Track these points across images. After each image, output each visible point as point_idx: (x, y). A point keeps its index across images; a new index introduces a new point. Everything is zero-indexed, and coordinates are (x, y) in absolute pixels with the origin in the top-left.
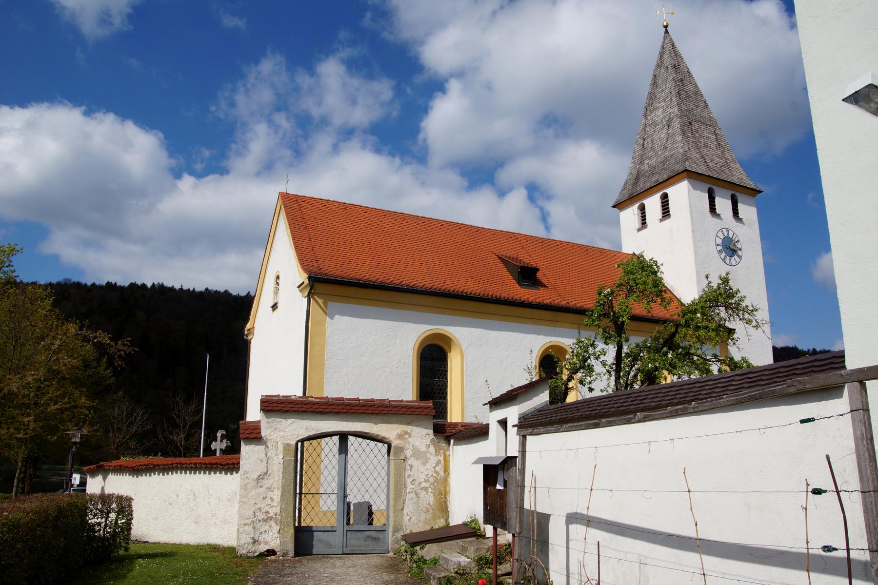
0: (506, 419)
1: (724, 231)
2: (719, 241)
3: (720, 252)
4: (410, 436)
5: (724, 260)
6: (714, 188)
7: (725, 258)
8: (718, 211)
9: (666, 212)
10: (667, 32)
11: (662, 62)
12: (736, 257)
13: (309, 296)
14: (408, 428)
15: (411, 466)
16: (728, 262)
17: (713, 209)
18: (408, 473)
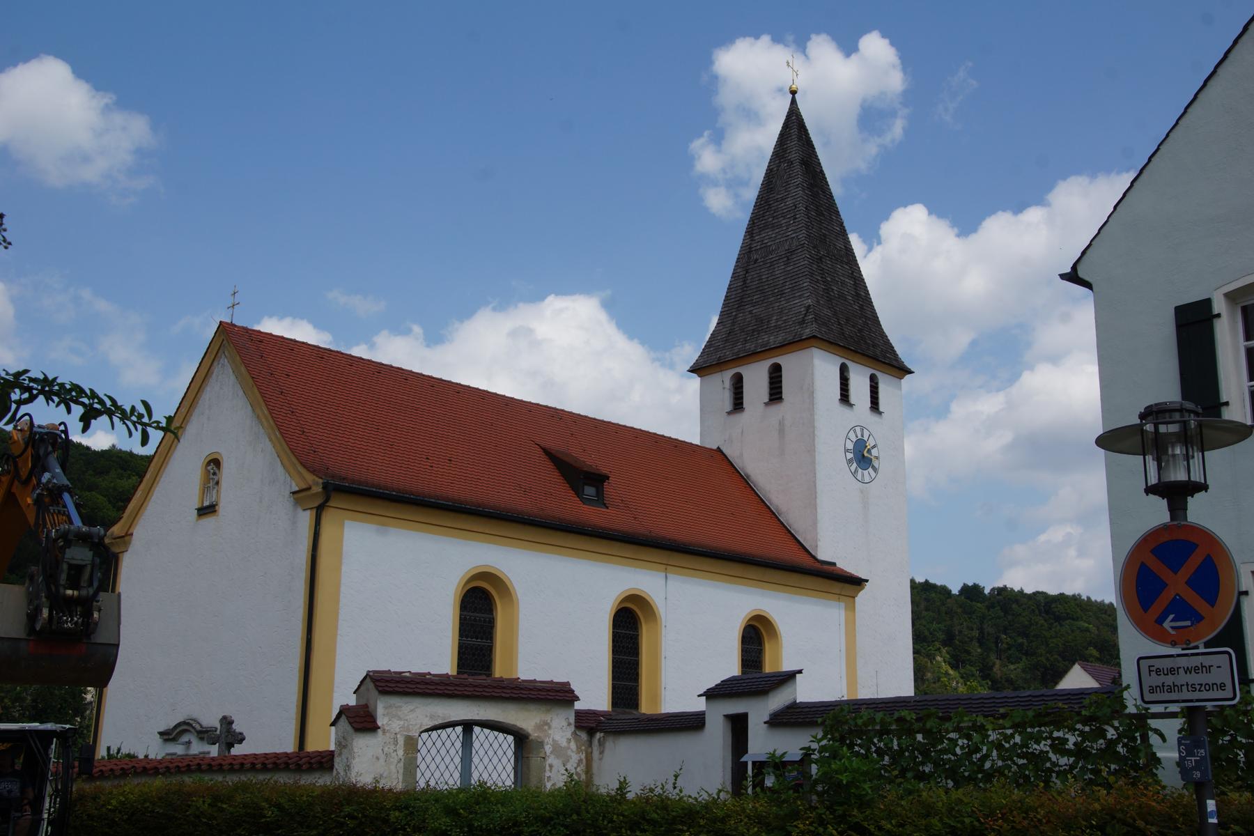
0: (726, 716)
1: (858, 429)
2: (850, 446)
4: (550, 728)
5: (854, 474)
6: (849, 364)
7: (856, 471)
8: (853, 399)
9: (776, 394)
10: (793, 102)
11: (785, 150)
12: (870, 470)
13: (319, 511)
14: (548, 717)
15: (551, 766)
16: (859, 477)
17: (845, 397)
18: (548, 774)
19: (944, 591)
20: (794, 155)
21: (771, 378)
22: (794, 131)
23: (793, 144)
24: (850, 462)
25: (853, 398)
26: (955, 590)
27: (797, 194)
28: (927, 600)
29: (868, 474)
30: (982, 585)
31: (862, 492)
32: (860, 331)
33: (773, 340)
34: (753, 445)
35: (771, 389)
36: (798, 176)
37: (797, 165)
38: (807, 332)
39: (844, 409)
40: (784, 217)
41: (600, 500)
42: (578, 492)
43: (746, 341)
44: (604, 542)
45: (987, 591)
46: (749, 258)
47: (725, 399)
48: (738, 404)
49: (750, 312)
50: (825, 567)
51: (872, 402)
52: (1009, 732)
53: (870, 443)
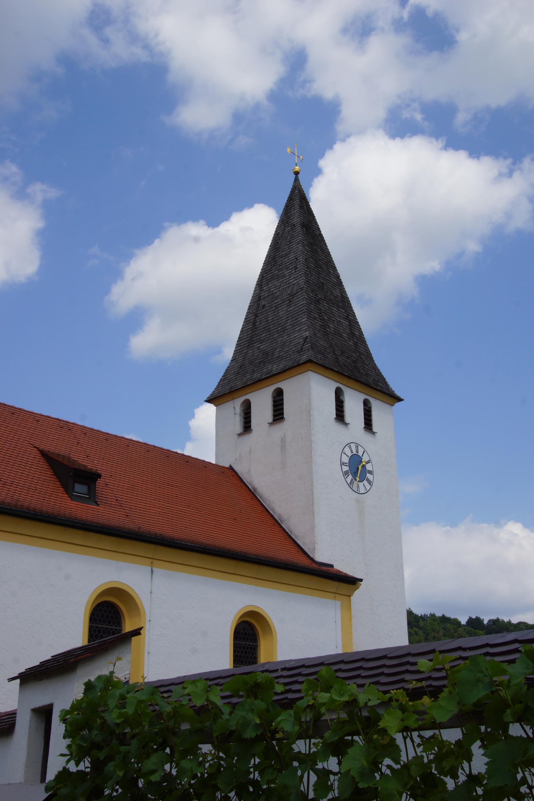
1: (353, 446)
2: (346, 460)
3: (346, 474)
5: (350, 485)
8: (347, 419)
9: (278, 415)
10: (297, 180)
11: (289, 218)
12: (365, 482)
17: (340, 416)
19: (456, 622)
20: (296, 220)
21: (274, 402)
22: (297, 202)
23: (296, 211)
24: (346, 474)
25: (348, 418)
26: (463, 621)
27: (298, 249)
28: (444, 629)
29: (363, 486)
30: (482, 618)
31: (357, 501)
32: (354, 362)
33: (275, 368)
34: (260, 461)
35: (275, 411)
36: (299, 234)
37: (299, 229)
38: (304, 358)
39: (339, 427)
40: (287, 269)
41: (92, 497)
42: (68, 490)
43: (254, 372)
44: (80, 532)
45: (485, 622)
46: (258, 305)
47: (237, 425)
48: (247, 427)
49: (259, 348)
50: (324, 568)
51: (366, 423)
52: (452, 735)
53: (365, 458)
